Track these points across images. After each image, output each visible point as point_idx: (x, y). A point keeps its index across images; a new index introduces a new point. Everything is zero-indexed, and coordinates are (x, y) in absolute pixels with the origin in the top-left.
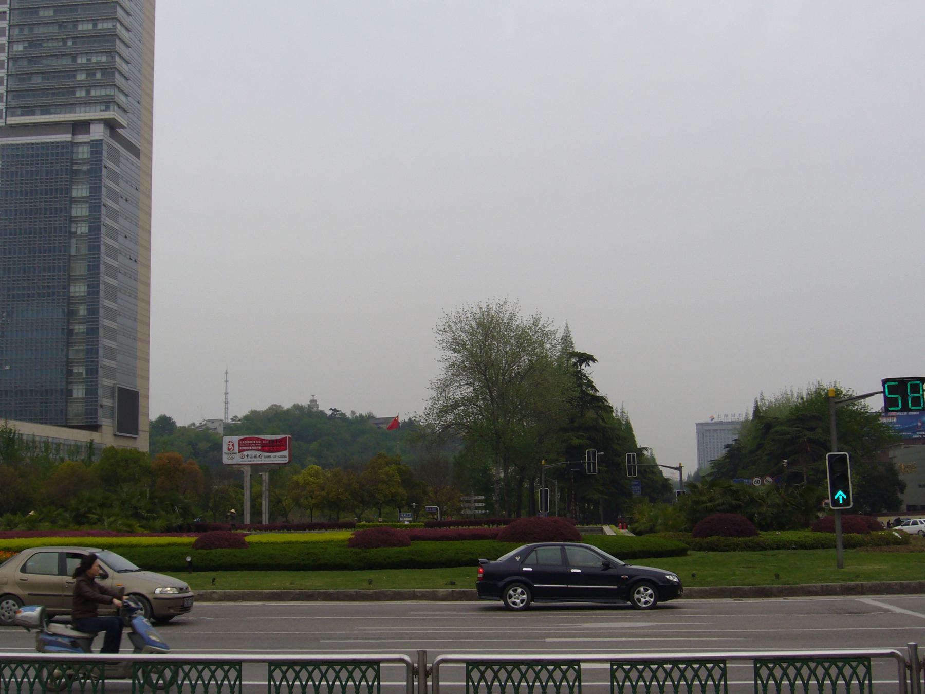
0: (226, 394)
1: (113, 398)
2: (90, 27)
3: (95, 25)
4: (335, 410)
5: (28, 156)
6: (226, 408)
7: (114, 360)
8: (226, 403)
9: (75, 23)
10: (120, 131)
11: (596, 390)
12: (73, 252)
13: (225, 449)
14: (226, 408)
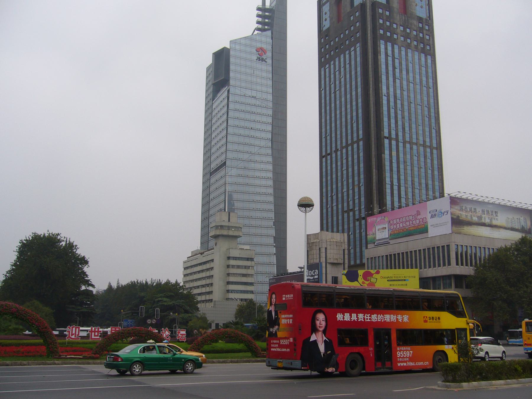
11: (93, 286)
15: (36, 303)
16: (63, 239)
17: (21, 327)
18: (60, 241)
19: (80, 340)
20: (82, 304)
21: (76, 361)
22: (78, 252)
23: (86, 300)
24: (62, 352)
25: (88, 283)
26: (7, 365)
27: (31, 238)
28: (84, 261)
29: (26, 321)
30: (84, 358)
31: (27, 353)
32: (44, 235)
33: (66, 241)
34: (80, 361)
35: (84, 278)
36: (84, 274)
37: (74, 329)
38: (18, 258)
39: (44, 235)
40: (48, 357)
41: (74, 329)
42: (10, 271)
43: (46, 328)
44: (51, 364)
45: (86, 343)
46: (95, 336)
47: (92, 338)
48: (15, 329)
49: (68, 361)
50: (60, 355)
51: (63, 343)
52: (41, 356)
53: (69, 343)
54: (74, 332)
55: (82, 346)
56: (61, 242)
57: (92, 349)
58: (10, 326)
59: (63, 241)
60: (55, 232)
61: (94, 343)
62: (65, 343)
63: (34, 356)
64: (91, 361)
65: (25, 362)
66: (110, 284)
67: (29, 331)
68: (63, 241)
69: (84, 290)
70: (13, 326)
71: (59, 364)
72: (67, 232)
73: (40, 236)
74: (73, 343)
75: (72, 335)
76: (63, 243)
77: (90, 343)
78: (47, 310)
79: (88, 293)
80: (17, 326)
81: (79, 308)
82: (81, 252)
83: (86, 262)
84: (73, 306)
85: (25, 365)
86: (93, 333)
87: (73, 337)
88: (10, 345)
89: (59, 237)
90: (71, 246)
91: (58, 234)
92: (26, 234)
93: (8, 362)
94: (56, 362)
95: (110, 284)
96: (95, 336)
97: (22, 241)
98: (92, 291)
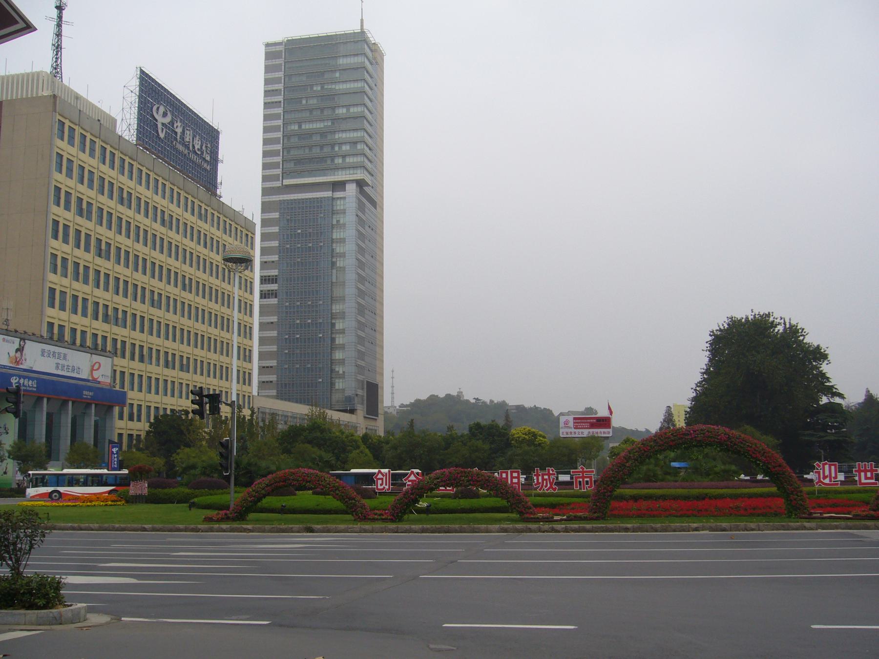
0: (393, 387)
1: (363, 389)
2: (344, 110)
3: (348, 110)
4: (477, 399)
5: (299, 208)
6: (393, 398)
7: (363, 360)
8: (393, 393)
9: (333, 108)
10: (366, 188)
11: (841, 396)
12: (334, 280)
13: (562, 424)
14: (393, 398)
15: (749, 428)
16: (778, 321)
17: (733, 467)
18: (773, 325)
19: (839, 487)
20: (825, 427)
21: (843, 523)
22: (807, 340)
23: (833, 420)
24: (814, 508)
25: (831, 391)
26: (724, 530)
27: (726, 326)
28: (819, 355)
29: (748, 460)
30: (856, 517)
31: (751, 510)
32: (747, 318)
33: (785, 324)
34: (849, 523)
35: (823, 383)
36: (823, 375)
37: (827, 467)
38: (710, 360)
39: (747, 318)
40: (790, 517)
41: (827, 467)
42: (700, 382)
43: (780, 466)
44: (797, 529)
45: (853, 492)
46: (866, 478)
47: (861, 483)
48: (724, 471)
49: (827, 523)
50: (811, 514)
51: (809, 493)
52: (776, 515)
53: (820, 492)
54: (827, 473)
55: (844, 496)
56: (776, 327)
57: (868, 503)
58: (716, 466)
59: (779, 324)
60: (763, 311)
61: (866, 491)
62: (813, 493)
63: (764, 515)
64: (870, 523)
65: (752, 525)
66: (868, 391)
67: (765, 476)
68: (779, 324)
69: (826, 404)
70: (720, 467)
71: (811, 529)
72: (784, 309)
73: (740, 320)
74: (828, 492)
75: (825, 477)
76: (780, 328)
77: (859, 491)
78: (770, 440)
79: (834, 409)
80: (727, 467)
81: (822, 434)
82: (811, 339)
83: (824, 357)
84: (810, 432)
85: (753, 530)
86: (863, 474)
87: (827, 481)
88: (721, 497)
89: (771, 319)
90: (793, 332)
91: (768, 315)
92: (718, 321)
93: (724, 525)
94: (807, 524)
95: (868, 391)
96: (866, 478)
97: (713, 332)
98: (840, 404)
